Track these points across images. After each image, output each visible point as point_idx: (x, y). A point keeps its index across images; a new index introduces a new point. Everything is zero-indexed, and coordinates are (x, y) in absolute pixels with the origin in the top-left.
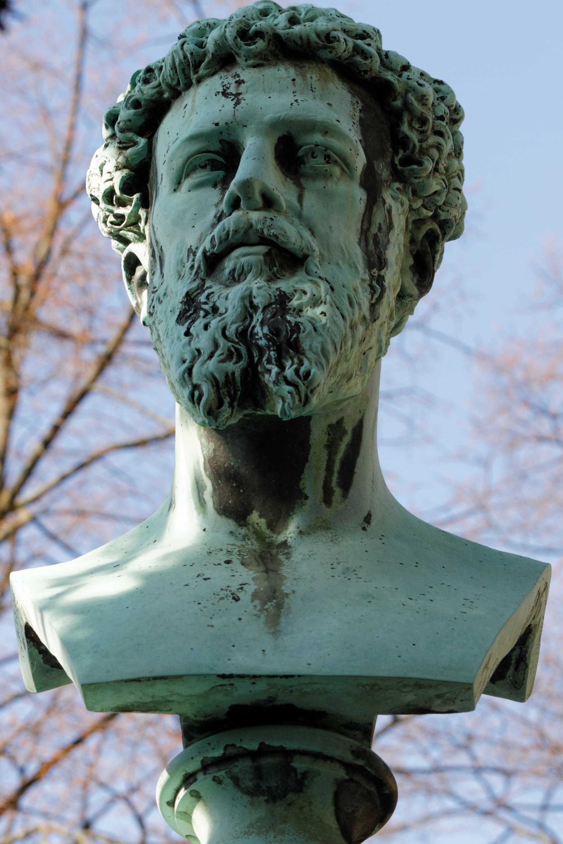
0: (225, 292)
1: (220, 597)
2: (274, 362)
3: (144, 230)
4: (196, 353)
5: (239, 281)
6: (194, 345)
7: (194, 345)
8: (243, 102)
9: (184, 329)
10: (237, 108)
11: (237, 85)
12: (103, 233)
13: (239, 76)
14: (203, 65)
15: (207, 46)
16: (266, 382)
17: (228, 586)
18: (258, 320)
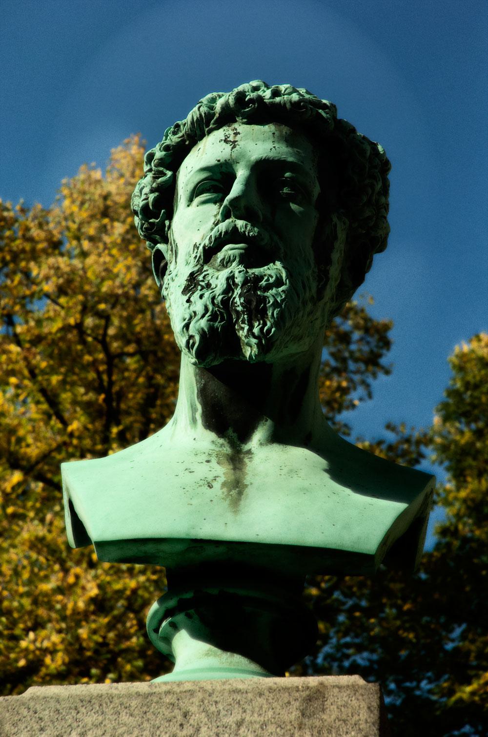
0: (216, 274)
1: (199, 484)
2: (246, 322)
3: (167, 233)
4: (193, 314)
5: (226, 267)
6: (193, 308)
7: (193, 308)
8: (237, 146)
9: (186, 298)
10: (233, 150)
11: (234, 135)
12: (141, 236)
13: (236, 130)
14: (212, 122)
15: (216, 109)
16: (241, 336)
17: (206, 478)
18: (238, 293)
